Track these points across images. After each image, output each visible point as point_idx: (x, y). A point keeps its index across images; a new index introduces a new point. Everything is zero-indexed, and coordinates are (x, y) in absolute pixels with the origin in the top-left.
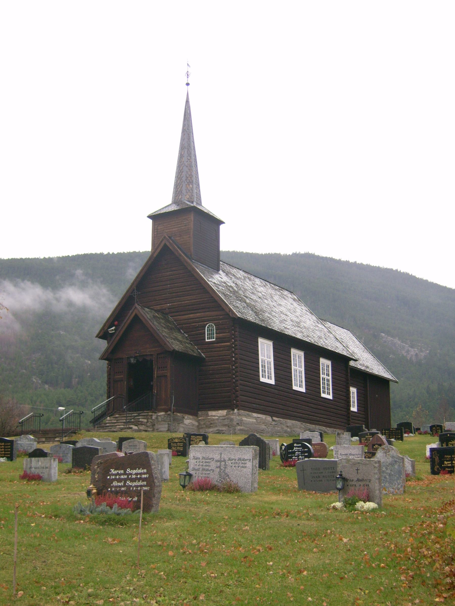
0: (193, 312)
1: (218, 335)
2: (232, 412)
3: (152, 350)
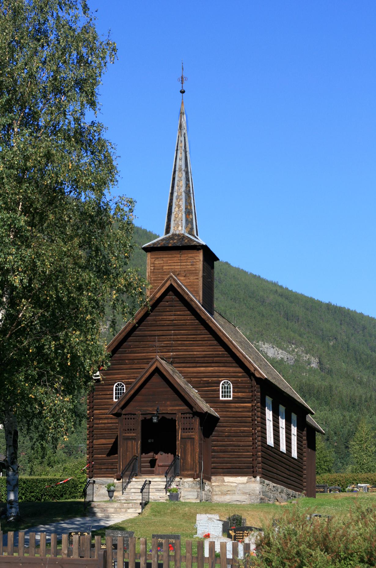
0: (204, 365)
1: (235, 394)
2: (253, 479)
3: (175, 408)
